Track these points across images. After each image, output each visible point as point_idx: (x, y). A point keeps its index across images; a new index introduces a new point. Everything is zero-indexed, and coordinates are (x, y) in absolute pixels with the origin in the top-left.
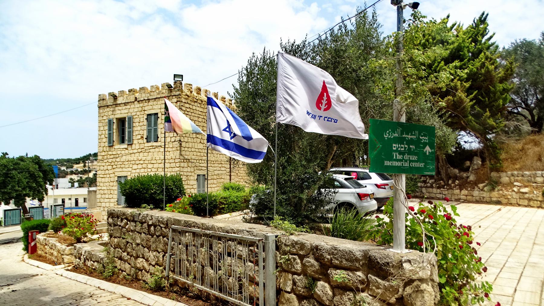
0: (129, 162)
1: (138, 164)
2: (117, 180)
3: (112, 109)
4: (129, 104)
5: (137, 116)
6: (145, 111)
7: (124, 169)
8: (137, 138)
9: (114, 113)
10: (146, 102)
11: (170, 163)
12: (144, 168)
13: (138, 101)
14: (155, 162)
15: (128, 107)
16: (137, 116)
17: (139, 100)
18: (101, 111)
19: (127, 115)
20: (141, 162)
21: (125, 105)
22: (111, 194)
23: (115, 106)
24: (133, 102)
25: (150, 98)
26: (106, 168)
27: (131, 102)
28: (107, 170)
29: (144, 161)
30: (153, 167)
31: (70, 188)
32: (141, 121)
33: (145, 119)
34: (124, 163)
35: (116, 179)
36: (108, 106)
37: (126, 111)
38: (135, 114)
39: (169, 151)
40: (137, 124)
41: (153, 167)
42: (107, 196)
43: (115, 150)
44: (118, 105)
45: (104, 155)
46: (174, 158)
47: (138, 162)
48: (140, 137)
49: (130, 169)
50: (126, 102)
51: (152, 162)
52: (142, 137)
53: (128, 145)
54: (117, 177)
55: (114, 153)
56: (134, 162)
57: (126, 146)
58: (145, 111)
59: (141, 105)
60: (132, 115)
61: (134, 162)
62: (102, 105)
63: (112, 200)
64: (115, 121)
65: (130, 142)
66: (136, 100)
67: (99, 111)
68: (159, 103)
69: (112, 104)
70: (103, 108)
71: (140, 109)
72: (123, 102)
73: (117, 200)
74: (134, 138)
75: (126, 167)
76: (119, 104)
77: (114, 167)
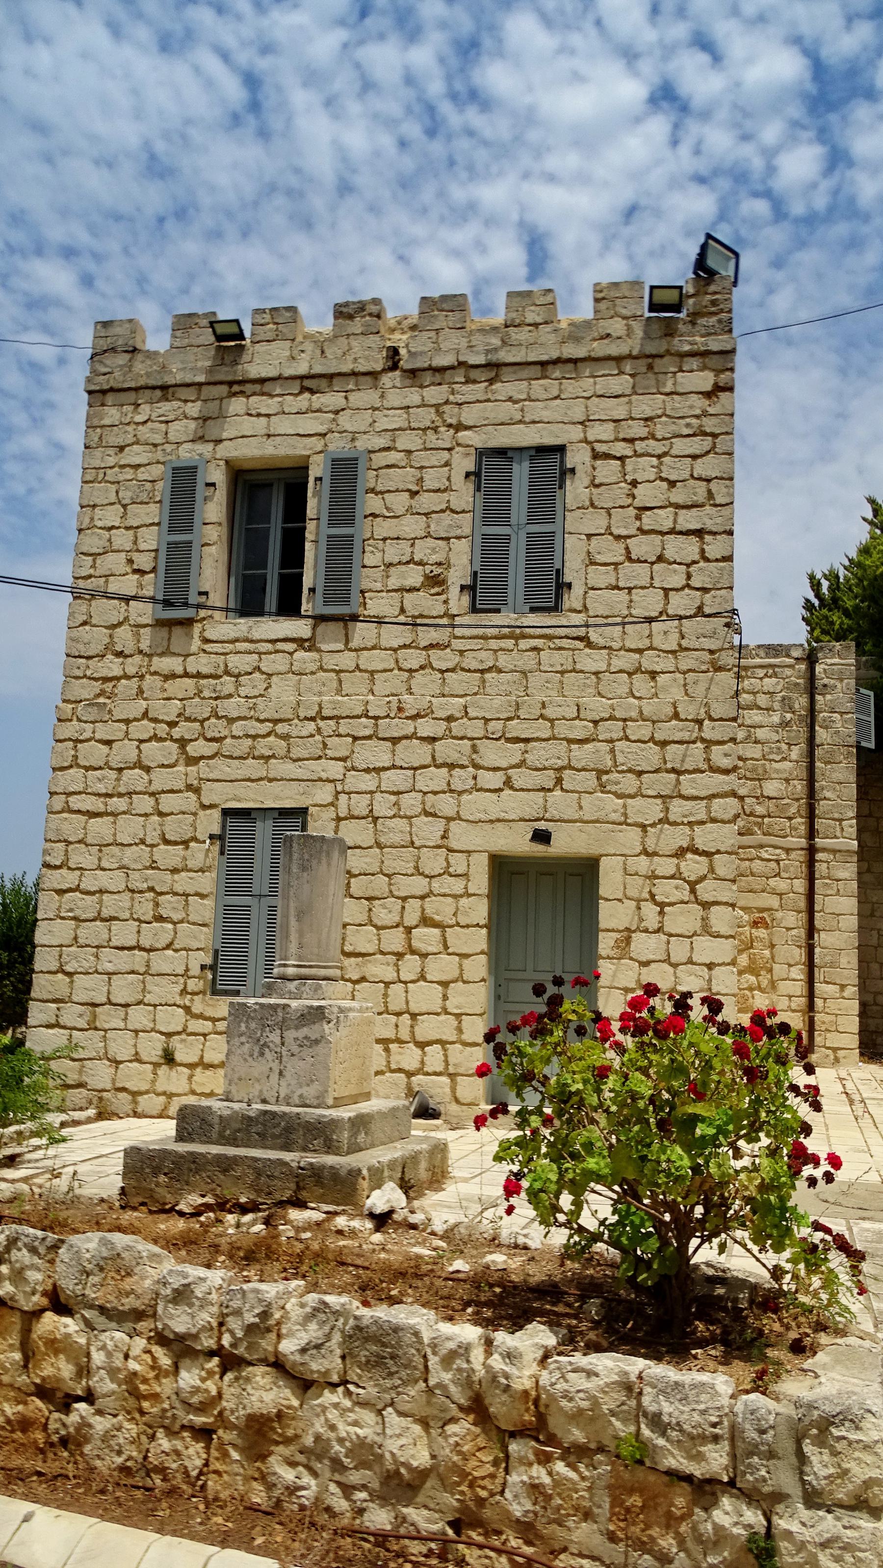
0: (328, 726)
1: (395, 741)
2: (216, 829)
3: (194, 409)
4: (337, 384)
5: (393, 457)
6: (459, 427)
7: (279, 768)
8: (393, 583)
9: (213, 434)
10: (468, 381)
11: (664, 744)
12: (451, 766)
13: (413, 373)
14: (542, 729)
15: (332, 399)
16: (393, 457)
17: (419, 363)
18: (112, 415)
19: (317, 444)
20: (426, 727)
21: (304, 389)
22: (160, 919)
23: (224, 389)
24: (373, 375)
25: (506, 356)
26: (127, 751)
27: (354, 374)
28: (139, 764)
29: (450, 719)
30: (522, 764)
31: (602, 856)
32: (428, 484)
33: (458, 479)
34: (281, 728)
35: (211, 822)
36: (165, 389)
37: (311, 424)
38: (382, 442)
39: (653, 675)
40: (399, 502)
41: (522, 764)
42: (124, 933)
43: (208, 647)
44: (249, 388)
45: (117, 671)
46: (688, 710)
47: (390, 728)
48: (414, 576)
49: (335, 769)
50: (318, 369)
51: (516, 728)
52: (435, 581)
53: (320, 619)
54: (216, 814)
55: (201, 664)
56: (364, 727)
57: (300, 628)
58: (459, 427)
59: (435, 394)
60: (362, 444)
61: (364, 727)
62: (118, 379)
63: (164, 962)
64: (218, 475)
65: (346, 600)
66: (394, 367)
67: (89, 418)
68: (571, 387)
69: (201, 378)
70: (131, 396)
71: (427, 417)
72: (288, 372)
73: (209, 961)
74: (368, 579)
75: (296, 753)
76: (262, 381)
77: (196, 748)
